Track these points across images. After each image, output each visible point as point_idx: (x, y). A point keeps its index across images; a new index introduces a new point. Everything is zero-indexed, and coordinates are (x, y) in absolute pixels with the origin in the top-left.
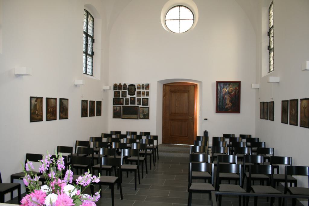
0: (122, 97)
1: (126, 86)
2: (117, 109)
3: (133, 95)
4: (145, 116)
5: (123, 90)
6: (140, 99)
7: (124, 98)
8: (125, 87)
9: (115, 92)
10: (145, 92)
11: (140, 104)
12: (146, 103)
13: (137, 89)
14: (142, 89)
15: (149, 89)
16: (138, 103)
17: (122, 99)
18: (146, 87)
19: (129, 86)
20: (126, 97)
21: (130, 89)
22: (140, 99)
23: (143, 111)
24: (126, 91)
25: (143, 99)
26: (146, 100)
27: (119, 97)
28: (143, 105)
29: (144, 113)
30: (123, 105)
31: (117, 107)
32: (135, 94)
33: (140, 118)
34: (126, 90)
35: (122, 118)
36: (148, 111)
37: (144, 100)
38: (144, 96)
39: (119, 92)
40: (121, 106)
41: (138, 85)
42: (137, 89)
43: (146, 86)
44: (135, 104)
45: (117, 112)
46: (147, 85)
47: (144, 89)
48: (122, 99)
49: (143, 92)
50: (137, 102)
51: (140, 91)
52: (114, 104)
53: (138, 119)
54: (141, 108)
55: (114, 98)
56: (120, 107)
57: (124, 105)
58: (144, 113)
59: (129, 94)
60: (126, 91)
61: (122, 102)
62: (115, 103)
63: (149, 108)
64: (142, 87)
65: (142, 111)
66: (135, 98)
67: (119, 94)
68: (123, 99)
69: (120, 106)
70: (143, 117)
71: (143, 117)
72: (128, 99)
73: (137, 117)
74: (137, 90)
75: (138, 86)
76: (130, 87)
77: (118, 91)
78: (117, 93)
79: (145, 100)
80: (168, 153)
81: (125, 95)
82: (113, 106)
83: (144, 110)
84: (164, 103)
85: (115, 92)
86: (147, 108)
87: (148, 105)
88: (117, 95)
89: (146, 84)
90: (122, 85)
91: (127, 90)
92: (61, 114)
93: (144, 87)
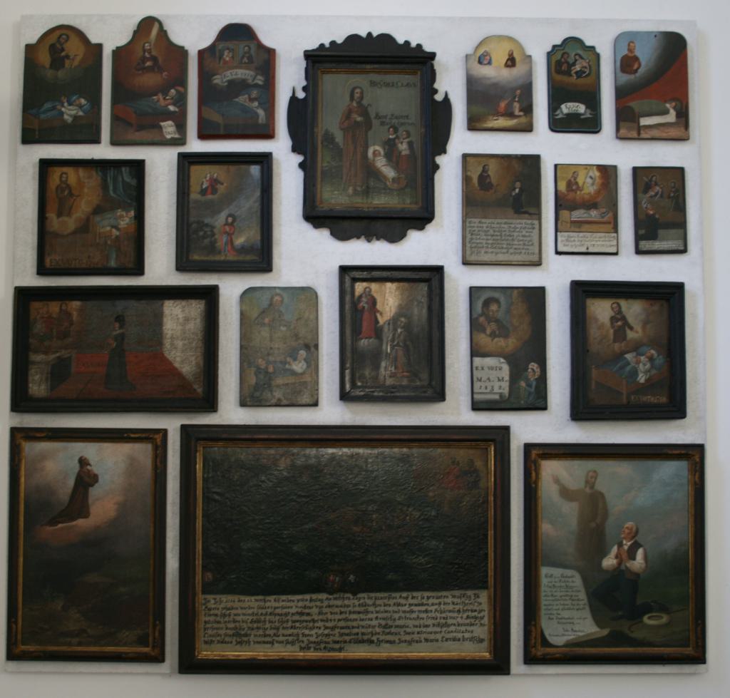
0: (183, 264)
1: (266, 60)
2: (86, 479)
3: (395, 237)
4: (636, 613)
5: (196, 146)
6: (535, 297)
7: (231, 288)
8: (239, 87)
9: (46, 166)
10: (608, 173)
11: (538, 402)
12: (643, 368)
13: (474, 124)
14: (558, 125)
15: (681, 129)
16: (497, 375)
17: (196, 308)
18: (622, 94)
19: (318, 60)
20: (261, 258)
21: (330, 122)
22: (535, 297)
23: (594, 505)
24: (265, 160)
25: (582, 292)
26: (634, 310)
27: (138, 268)
28: (582, 410)
29: (609, 562)
30: (209, 402)
31: (90, 450)
32: (423, 217)
33: (538, 654)
34: (268, 134)
35: (191, 665)
36: (683, 521)
37: (601, 310)
38: (598, 241)
39: (138, 167)
40: (172, 424)
41: (484, 59)
42: (474, 124)
43: (627, 63)
44: (437, 393)
45: (96, 543)
46: (646, 56)
47: (590, 125)
48: (196, 308)
49: (589, 186)
50: (476, 351)
51: (531, 163)
52: (38, 388)
53: (497, 665)
54: (551, 469)
55: (32, 280)
56: (142, 451)
57: (231, 412)
58: (609, 562)
59: (315, 216)
60: (265, 160)
61: (183, 358)
62: (59, 373)
63: (693, 455)
64: (557, 96)
65: (570, 511)
66: (431, 277)
67: (125, 219)
68: (210, 296)
69: (156, 439)
70: (586, 627)
71: (586, 627)
72: (307, 295)
73: (482, 631)
74: (462, 141)
75: (487, 72)
76: (337, 85)
77: (104, 151)
78: (89, 193)
79: (619, 319)
80: (646, 672)
81: (246, 237)
82: (18, 436)
83: (617, 503)
84: (347, 307)
85: (46, 166)
86: (671, 470)
87: (675, 407)
88: (85, 227)
89: (627, 41)
90: (182, 53)
91: (280, 147)
92: (516, 291)
93: (593, 100)
